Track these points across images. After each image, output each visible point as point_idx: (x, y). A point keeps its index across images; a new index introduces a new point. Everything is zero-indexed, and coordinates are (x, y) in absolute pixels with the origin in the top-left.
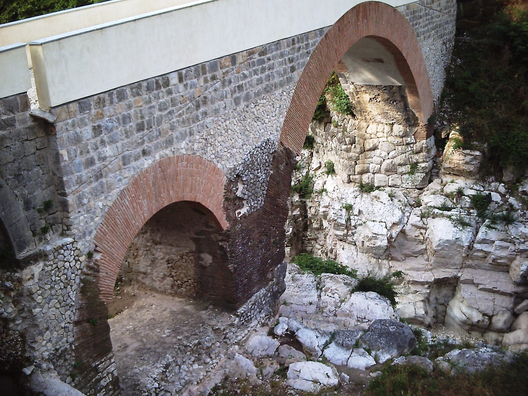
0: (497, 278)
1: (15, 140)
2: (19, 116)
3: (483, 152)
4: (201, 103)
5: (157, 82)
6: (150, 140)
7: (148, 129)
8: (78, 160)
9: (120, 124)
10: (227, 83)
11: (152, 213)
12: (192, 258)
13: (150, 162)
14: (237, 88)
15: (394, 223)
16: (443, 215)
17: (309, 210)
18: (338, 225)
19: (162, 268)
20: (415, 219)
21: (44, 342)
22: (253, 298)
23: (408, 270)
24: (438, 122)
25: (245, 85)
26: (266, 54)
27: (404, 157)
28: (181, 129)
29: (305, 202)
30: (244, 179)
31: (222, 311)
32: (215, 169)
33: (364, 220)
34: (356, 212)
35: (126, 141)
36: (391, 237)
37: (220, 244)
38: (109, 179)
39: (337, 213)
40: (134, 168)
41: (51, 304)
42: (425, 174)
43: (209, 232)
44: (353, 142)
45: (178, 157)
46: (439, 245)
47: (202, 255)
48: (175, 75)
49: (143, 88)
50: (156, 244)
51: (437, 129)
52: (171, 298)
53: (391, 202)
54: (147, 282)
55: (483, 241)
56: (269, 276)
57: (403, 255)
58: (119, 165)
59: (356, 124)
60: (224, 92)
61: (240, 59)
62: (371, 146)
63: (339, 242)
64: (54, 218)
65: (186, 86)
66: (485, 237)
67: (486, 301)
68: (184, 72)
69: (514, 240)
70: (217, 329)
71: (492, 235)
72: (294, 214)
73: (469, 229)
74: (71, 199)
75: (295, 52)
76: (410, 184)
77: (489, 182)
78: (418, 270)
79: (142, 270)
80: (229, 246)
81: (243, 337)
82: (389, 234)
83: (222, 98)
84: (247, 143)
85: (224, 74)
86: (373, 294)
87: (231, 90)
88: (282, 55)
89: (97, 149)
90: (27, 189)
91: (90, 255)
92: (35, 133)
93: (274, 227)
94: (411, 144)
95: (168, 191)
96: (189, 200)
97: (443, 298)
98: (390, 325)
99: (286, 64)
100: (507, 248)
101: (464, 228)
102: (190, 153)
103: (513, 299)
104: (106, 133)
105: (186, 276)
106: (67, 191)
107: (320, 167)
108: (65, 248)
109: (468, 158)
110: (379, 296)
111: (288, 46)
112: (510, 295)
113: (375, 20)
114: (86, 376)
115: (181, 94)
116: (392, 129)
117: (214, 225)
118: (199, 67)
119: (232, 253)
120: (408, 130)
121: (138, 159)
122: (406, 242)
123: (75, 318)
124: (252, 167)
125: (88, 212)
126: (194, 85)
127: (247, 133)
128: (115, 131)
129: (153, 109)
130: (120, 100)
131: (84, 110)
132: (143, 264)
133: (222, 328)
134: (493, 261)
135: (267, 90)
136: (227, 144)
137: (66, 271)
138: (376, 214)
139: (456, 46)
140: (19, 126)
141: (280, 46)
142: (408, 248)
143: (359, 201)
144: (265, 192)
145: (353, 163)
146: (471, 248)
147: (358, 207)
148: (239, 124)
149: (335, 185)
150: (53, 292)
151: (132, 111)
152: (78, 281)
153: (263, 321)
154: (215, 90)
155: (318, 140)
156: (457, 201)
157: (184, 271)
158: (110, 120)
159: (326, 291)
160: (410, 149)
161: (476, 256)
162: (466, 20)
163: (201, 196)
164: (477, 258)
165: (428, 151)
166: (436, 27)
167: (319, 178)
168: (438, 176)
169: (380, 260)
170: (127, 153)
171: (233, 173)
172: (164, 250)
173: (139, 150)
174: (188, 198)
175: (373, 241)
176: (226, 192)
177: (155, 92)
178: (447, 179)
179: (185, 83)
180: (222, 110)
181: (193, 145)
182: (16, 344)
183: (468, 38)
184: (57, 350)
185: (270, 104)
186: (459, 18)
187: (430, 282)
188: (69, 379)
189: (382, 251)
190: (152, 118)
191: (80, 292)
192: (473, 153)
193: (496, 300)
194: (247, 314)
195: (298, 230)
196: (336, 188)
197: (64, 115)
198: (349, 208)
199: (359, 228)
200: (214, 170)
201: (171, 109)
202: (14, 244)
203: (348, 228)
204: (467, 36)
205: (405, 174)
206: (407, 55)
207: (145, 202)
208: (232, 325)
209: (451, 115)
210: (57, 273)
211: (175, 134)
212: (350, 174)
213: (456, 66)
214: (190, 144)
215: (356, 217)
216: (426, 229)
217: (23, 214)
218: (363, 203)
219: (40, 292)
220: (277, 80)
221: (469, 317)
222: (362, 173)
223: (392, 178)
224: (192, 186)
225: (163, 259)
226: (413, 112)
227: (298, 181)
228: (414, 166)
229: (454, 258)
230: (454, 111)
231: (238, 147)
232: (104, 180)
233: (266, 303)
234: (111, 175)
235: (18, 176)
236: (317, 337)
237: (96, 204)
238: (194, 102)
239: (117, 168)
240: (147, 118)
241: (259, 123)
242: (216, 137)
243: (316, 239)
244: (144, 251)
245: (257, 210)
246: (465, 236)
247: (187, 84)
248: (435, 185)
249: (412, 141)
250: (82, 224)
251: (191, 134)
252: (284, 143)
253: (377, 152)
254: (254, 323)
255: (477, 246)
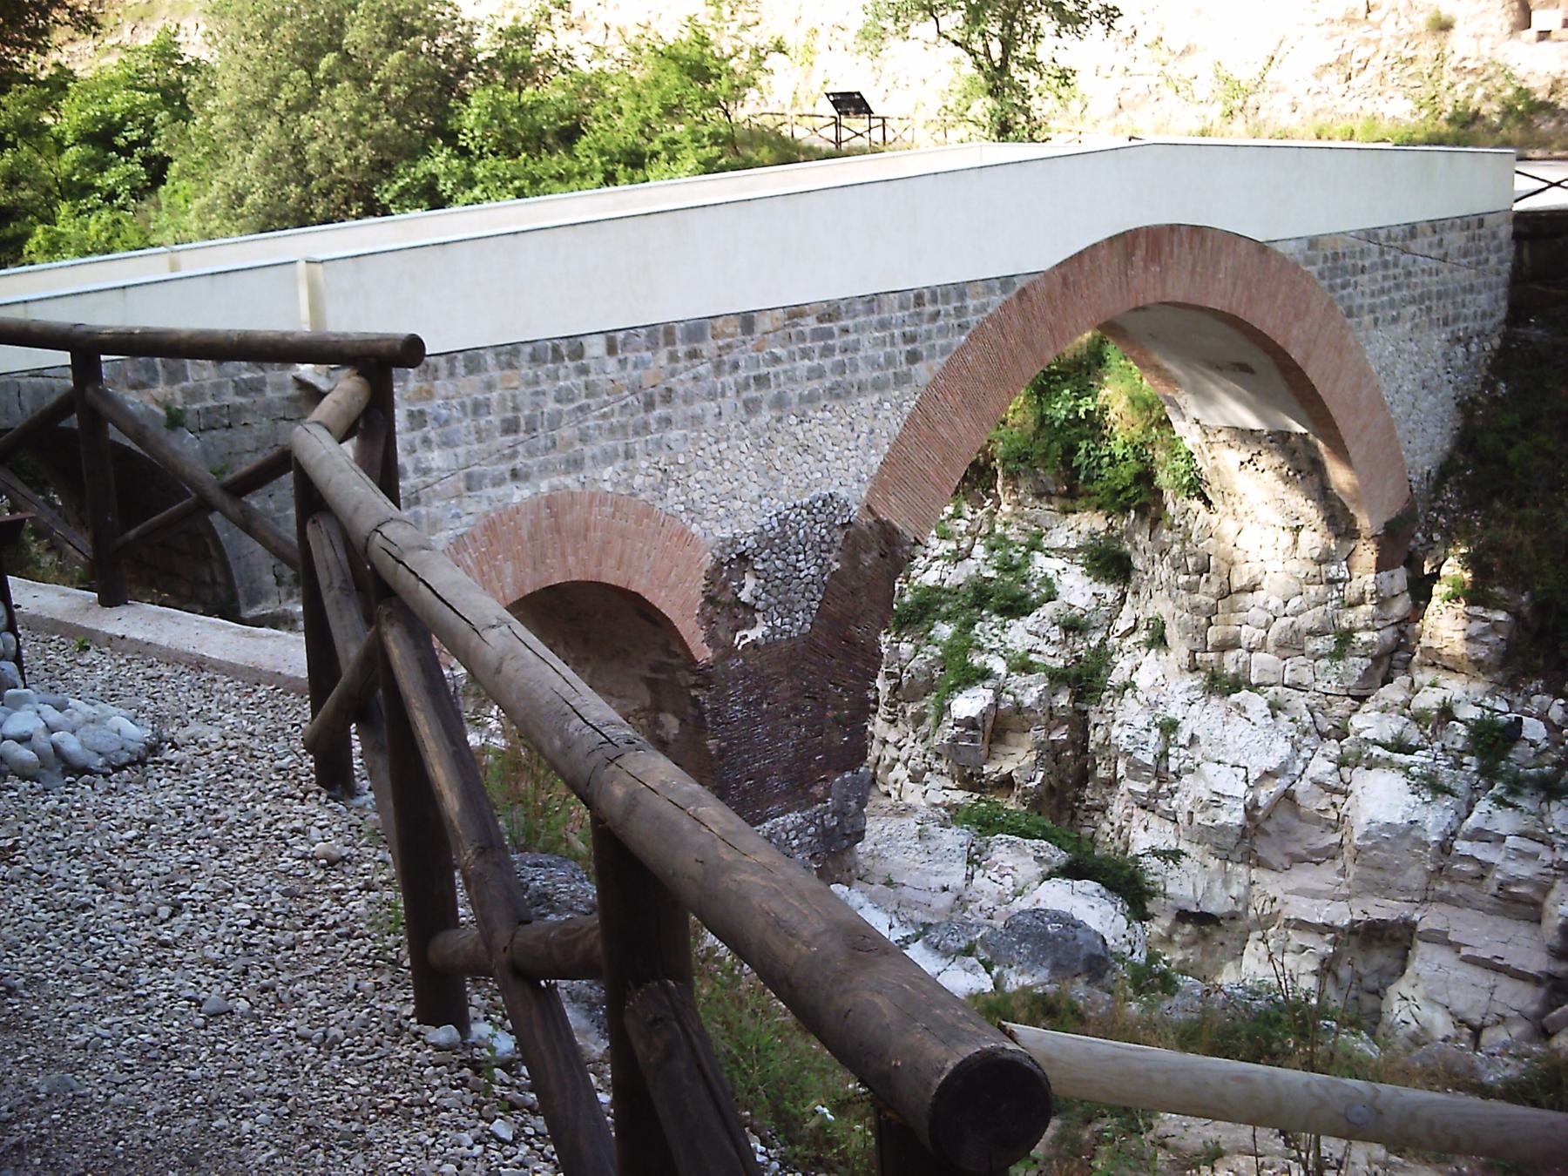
0: (1510, 934)
3: (1516, 615)
4: (657, 399)
5: (556, 349)
6: (531, 453)
7: (525, 432)
10: (727, 368)
12: (643, 721)
13: (527, 493)
14: (752, 381)
15: (1266, 772)
16: (1392, 763)
17: (1092, 732)
18: (1137, 768)
20: (1321, 767)
23: (1293, 893)
24: (1419, 535)
25: (776, 376)
26: (838, 318)
27: (1320, 615)
28: (606, 443)
29: (1086, 712)
30: (759, 566)
33: (1198, 759)
34: (1183, 739)
35: (476, 447)
36: (1255, 805)
37: (693, 693)
38: (432, 510)
39: (1137, 736)
42: (1370, 662)
43: (671, 665)
44: (1203, 569)
45: (593, 496)
46: (1366, 836)
48: (601, 339)
51: (1415, 549)
53: (1270, 721)
55: (1479, 835)
56: (819, 790)
57: (1286, 854)
58: (457, 489)
59: (1213, 525)
60: (719, 386)
61: (764, 324)
62: (1245, 581)
63: (1138, 812)
65: (623, 363)
66: (1482, 825)
67: (1473, 989)
68: (621, 335)
69: (1553, 837)
71: (1504, 821)
72: (1053, 737)
73: (1448, 801)
75: (921, 321)
76: (1334, 684)
77: (1526, 693)
78: (1315, 895)
80: (711, 698)
82: (1250, 796)
83: (712, 396)
84: (772, 493)
85: (720, 348)
86: (1090, 886)
87: (736, 383)
88: (883, 325)
89: (414, 451)
90: (275, 502)
93: (836, 686)
94: (1340, 581)
95: (563, 555)
96: (613, 583)
97: (1376, 976)
98: (1052, 921)
99: (893, 344)
100: (1535, 856)
101: (1434, 799)
103: (1541, 992)
104: (436, 426)
107: (1133, 630)
109: (1477, 626)
110: (1103, 891)
111: (902, 307)
112: (1535, 980)
113: (1189, 266)
115: (610, 377)
116: (1296, 542)
117: (679, 651)
118: (657, 331)
120: (1333, 547)
122: (1296, 823)
124: (782, 546)
127: (773, 473)
128: (454, 425)
129: (542, 397)
134: (1500, 889)
135: (835, 392)
136: (720, 489)
138: (1228, 747)
139: (1501, 352)
140: (269, 393)
141: (879, 306)
142: (1299, 840)
143: (1197, 713)
144: (815, 605)
145: (1204, 620)
146: (1447, 850)
147: (1190, 726)
148: (755, 453)
149: (1159, 674)
151: (494, 396)
154: (695, 378)
155: (1138, 562)
156: (1433, 731)
158: (446, 406)
159: (985, 868)
160: (1336, 594)
161: (1459, 871)
162: (1538, 287)
164: (1463, 878)
165: (1383, 603)
166: (1422, 298)
167: (1127, 656)
168: (1406, 667)
169: (1229, 865)
170: (476, 468)
171: (728, 550)
173: (505, 468)
174: (611, 577)
175: (1211, 811)
176: (706, 586)
177: (550, 366)
178: (1424, 677)
179: (621, 356)
180: (709, 419)
181: (632, 477)
183: (1539, 332)
185: (843, 421)
186: (1517, 280)
187: (1337, 927)
189: (1231, 840)
190: (539, 413)
192: (1488, 615)
193: (1497, 991)
195: (1062, 781)
196: (1161, 680)
198: (1169, 727)
199: (1187, 779)
200: (682, 534)
201: (583, 401)
202: (240, 591)
203: (1160, 775)
204: (1537, 326)
205: (1322, 656)
206: (1308, 355)
207: (508, 569)
209: (1455, 519)
211: (588, 451)
212: (1193, 648)
213: (1494, 400)
214: (625, 475)
215: (1182, 752)
216: (1346, 794)
218: (1204, 718)
220: (865, 374)
221: (1426, 1025)
222: (1224, 647)
223: (1293, 666)
224: (621, 557)
226: (1341, 502)
227: (1076, 658)
228: (1345, 638)
229: (1405, 873)
230: (1464, 509)
231: (748, 498)
232: (423, 510)
233: (800, 845)
236: (890, 927)
238: (640, 396)
239: (452, 492)
240: (527, 412)
241: (810, 459)
242: (691, 472)
243: (1103, 809)
245: (789, 638)
246: (1435, 818)
247: (626, 359)
248: (1393, 692)
249: (1342, 574)
251: (628, 455)
252: (877, 508)
253: (1259, 596)
255: (1462, 846)
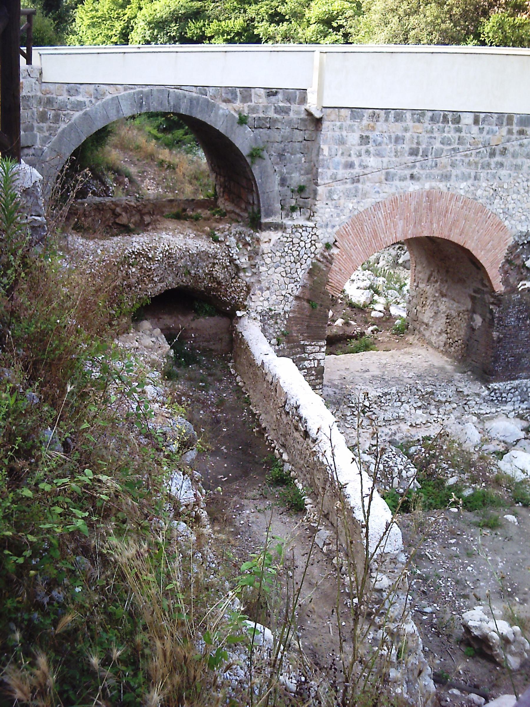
1: (286, 126)
2: (294, 107)
4: (498, 152)
5: (445, 117)
8: (337, 159)
9: (391, 142)
11: (406, 236)
12: (466, 317)
19: (441, 324)
21: (262, 299)
22: (517, 382)
28: (465, 170)
31: (477, 379)
32: (503, 229)
35: (394, 159)
37: (491, 307)
40: (396, 186)
41: (277, 270)
45: (453, 196)
47: (475, 316)
49: (426, 117)
50: (443, 296)
52: (441, 355)
54: (427, 334)
58: (380, 178)
64: (305, 203)
65: (481, 130)
68: (482, 116)
70: (461, 392)
74: (321, 190)
79: (426, 321)
80: (499, 311)
81: (486, 413)
90: (286, 169)
91: (328, 246)
92: (305, 126)
96: (456, 242)
102: (469, 195)
105: (457, 336)
106: (319, 181)
108: (304, 229)
114: (291, 348)
115: (473, 136)
119: (500, 320)
121: (403, 181)
123: (296, 293)
125: (336, 207)
126: (492, 132)
130: (397, 121)
131: (355, 118)
132: (427, 316)
133: (465, 393)
137: (299, 249)
140: (292, 115)
150: (283, 261)
152: (309, 262)
153: (521, 412)
154: (521, 145)
157: (457, 330)
163: (473, 244)
172: (447, 304)
173: (408, 172)
177: (440, 124)
179: (481, 127)
181: (476, 190)
182: (241, 292)
184: (271, 310)
188: (274, 341)
190: (431, 148)
191: (308, 273)
194: (501, 394)
197: (333, 117)
200: (498, 225)
201: (456, 146)
207: (401, 223)
208: (478, 395)
210: (291, 247)
211: (454, 172)
214: (472, 188)
217: (277, 188)
219: (270, 255)
225: (444, 313)
232: (360, 186)
234: (368, 184)
235: (281, 156)
237: (346, 204)
239: (377, 180)
240: (424, 146)
244: (431, 301)
250: (327, 216)
254: (509, 407)
